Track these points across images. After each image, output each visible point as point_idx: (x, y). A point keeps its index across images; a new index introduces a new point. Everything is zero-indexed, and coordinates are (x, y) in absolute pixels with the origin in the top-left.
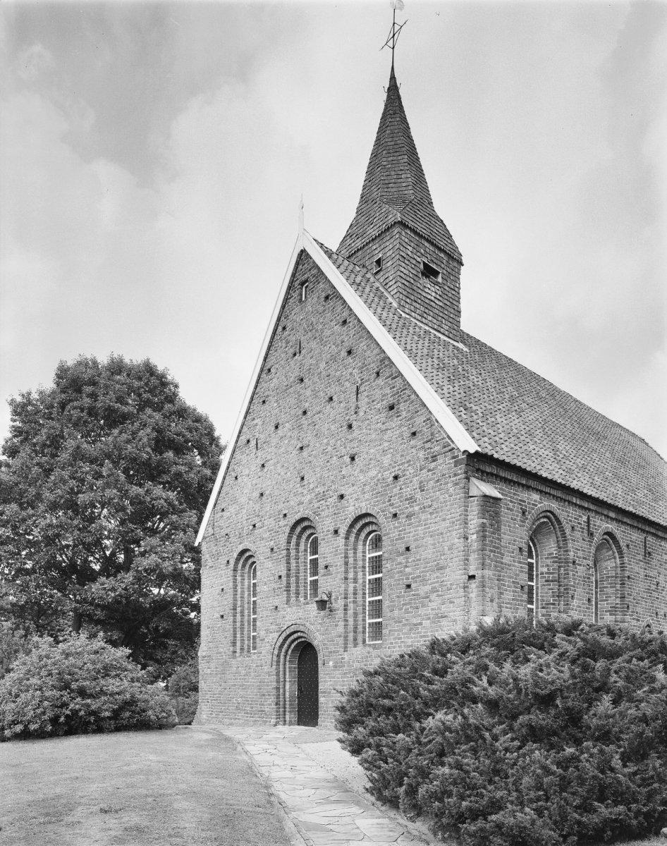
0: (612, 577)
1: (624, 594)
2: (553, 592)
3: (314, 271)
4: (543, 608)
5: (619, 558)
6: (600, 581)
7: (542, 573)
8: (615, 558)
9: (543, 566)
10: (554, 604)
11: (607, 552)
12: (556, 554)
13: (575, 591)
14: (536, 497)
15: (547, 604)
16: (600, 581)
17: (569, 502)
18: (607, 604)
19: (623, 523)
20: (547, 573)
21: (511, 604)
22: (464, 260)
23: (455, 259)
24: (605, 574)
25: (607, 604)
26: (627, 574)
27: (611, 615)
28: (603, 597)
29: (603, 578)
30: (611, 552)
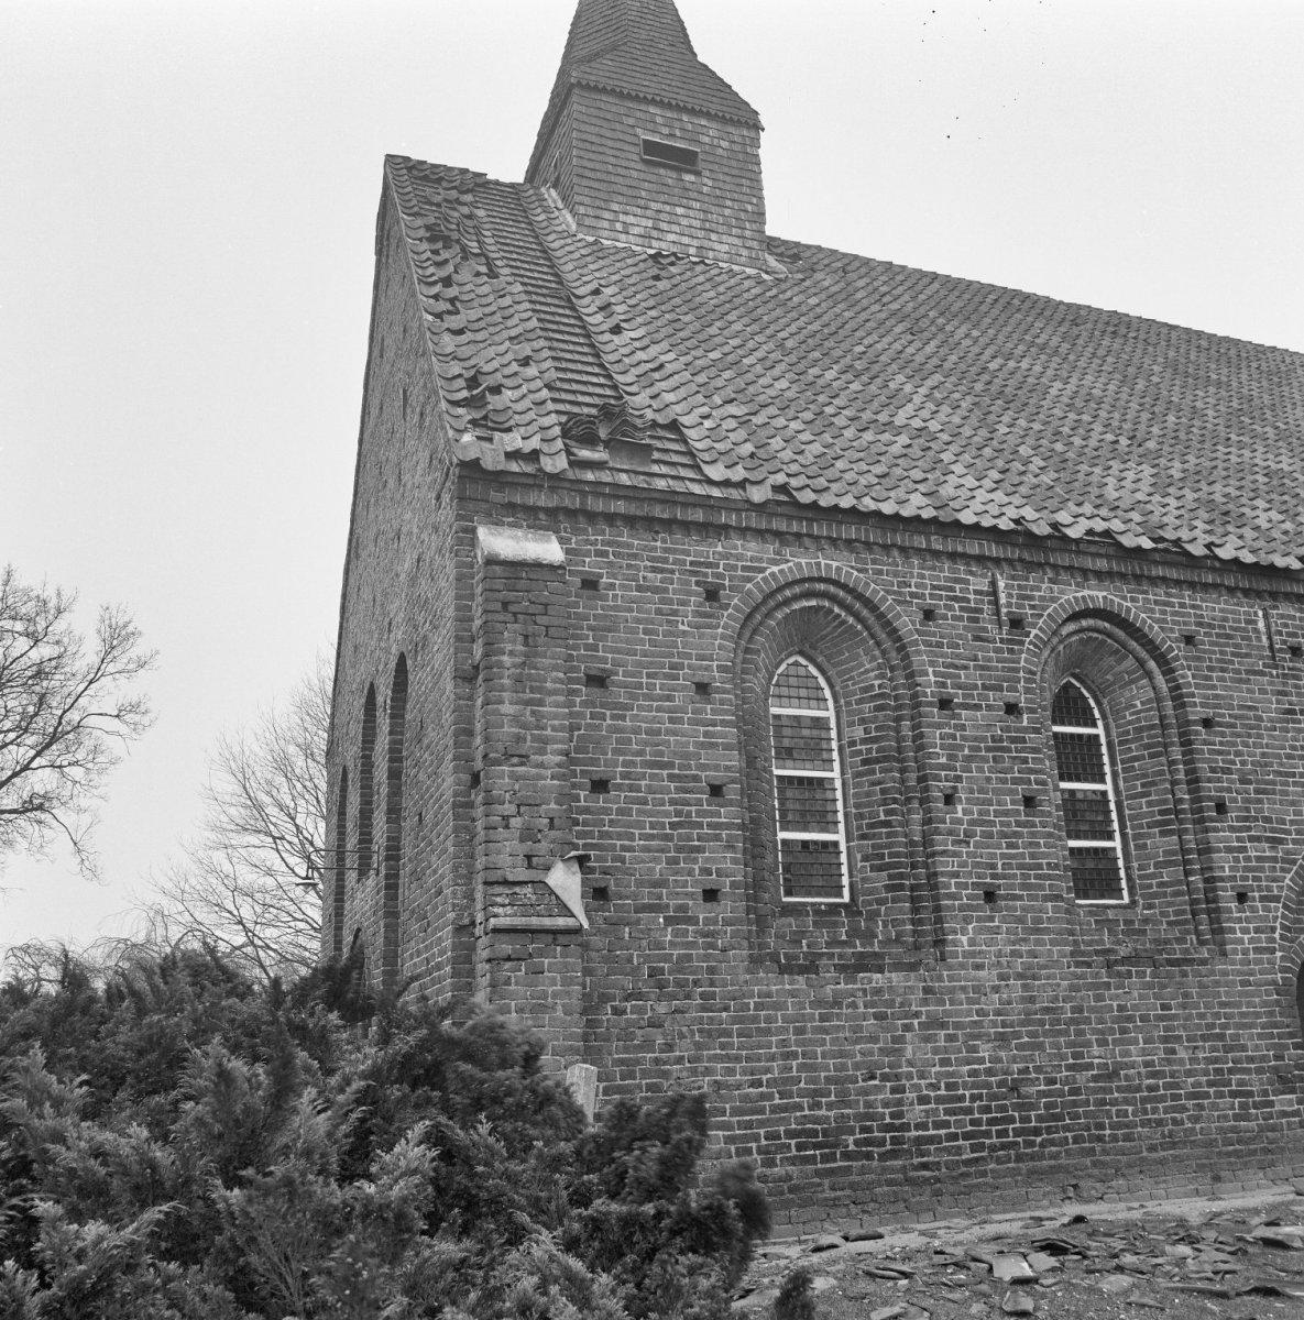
0: (1153, 727)
1: (1194, 771)
2: (883, 791)
3: (1144, 326)
4: (863, 837)
5: (1164, 674)
6: (1121, 743)
7: (852, 743)
8: (1149, 675)
9: (851, 724)
10: (887, 824)
11: (1119, 662)
12: (880, 686)
13: (958, 779)
14: (750, 549)
15: (871, 826)
16: (1121, 743)
17: (903, 550)
18: (1149, 804)
19: (1154, 581)
20: (864, 741)
21: (668, 838)
22: (763, 120)
23: (744, 120)
24: (1130, 723)
25: (1149, 804)
26: (1196, 713)
27: (1163, 833)
28: (1135, 787)
29: (1128, 732)
30: (1130, 662)
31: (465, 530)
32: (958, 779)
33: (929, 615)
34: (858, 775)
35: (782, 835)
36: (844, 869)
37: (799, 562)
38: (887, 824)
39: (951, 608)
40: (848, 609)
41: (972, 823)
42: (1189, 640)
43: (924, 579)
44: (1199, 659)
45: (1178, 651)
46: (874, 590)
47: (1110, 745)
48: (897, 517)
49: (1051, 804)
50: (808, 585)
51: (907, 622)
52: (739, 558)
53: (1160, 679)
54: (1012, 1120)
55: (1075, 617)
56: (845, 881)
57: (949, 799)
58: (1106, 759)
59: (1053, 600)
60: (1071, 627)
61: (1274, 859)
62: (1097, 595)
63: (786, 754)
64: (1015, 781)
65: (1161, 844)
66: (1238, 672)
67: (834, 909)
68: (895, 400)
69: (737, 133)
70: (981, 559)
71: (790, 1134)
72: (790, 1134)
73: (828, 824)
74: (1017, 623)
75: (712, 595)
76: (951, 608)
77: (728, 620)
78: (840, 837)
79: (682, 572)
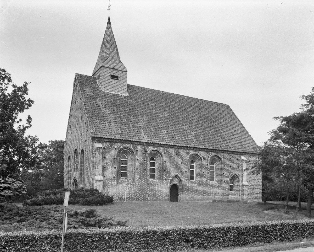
10: (131, 171)
13: (138, 167)
14: (119, 144)
22: (128, 70)
31: (93, 143)
32: (138, 167)
33: (137, 151)
34: (129, 166)
35: (121, 172)
36: (127, 175)
37: (124, 146)
38: (131, 171)
39: (139, 150)
40: (129, 150)
41: (139, 171)
42: (165, 153)
43: (137, 147)
44: (165, 155)
45: (163, 154)
46: (132, 148)
47: (156, 163)
48: (135, 141)
49: (210, 173)
50: (125, 148)
51: (135, 152)
52: (119, 145)
53: (161, 157)
54: (140, 198)
55: (153, 151)
56: (127, 176)
57: (137, 169)
58: (155, 165)
59: (150, 149)
60: (152, 151)
61: (170, 176)
62: (155, 148)
63: (122, 164)
64: (144, 167)
65: (159, 174)
66: (169, 156)
67: (125, 179)
68: (139, 121)
69: (124, 73)
70: (143, 145)
71: (120, 197)
72: (120, 197)
73: (126, 171)
74: (146, 151)
75: (116, 149)
76: (139, 150)
77: (117, 151)
78: (127, 172)
79: (113, 147)
